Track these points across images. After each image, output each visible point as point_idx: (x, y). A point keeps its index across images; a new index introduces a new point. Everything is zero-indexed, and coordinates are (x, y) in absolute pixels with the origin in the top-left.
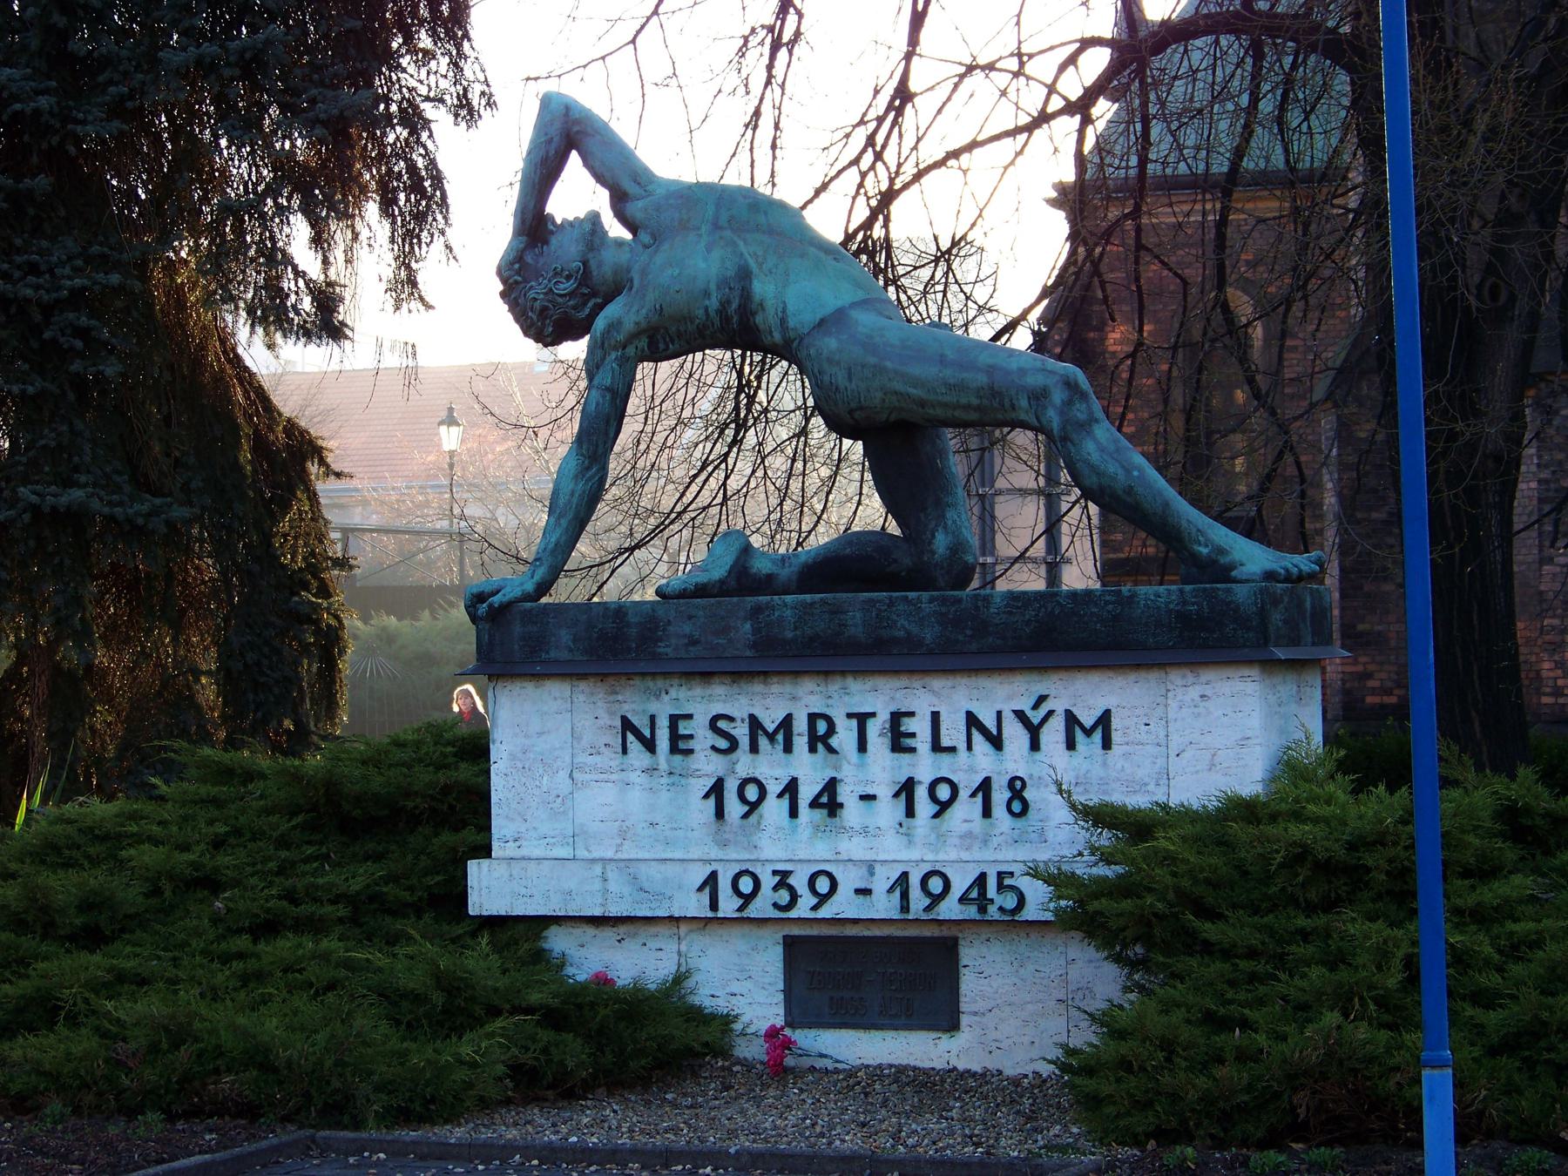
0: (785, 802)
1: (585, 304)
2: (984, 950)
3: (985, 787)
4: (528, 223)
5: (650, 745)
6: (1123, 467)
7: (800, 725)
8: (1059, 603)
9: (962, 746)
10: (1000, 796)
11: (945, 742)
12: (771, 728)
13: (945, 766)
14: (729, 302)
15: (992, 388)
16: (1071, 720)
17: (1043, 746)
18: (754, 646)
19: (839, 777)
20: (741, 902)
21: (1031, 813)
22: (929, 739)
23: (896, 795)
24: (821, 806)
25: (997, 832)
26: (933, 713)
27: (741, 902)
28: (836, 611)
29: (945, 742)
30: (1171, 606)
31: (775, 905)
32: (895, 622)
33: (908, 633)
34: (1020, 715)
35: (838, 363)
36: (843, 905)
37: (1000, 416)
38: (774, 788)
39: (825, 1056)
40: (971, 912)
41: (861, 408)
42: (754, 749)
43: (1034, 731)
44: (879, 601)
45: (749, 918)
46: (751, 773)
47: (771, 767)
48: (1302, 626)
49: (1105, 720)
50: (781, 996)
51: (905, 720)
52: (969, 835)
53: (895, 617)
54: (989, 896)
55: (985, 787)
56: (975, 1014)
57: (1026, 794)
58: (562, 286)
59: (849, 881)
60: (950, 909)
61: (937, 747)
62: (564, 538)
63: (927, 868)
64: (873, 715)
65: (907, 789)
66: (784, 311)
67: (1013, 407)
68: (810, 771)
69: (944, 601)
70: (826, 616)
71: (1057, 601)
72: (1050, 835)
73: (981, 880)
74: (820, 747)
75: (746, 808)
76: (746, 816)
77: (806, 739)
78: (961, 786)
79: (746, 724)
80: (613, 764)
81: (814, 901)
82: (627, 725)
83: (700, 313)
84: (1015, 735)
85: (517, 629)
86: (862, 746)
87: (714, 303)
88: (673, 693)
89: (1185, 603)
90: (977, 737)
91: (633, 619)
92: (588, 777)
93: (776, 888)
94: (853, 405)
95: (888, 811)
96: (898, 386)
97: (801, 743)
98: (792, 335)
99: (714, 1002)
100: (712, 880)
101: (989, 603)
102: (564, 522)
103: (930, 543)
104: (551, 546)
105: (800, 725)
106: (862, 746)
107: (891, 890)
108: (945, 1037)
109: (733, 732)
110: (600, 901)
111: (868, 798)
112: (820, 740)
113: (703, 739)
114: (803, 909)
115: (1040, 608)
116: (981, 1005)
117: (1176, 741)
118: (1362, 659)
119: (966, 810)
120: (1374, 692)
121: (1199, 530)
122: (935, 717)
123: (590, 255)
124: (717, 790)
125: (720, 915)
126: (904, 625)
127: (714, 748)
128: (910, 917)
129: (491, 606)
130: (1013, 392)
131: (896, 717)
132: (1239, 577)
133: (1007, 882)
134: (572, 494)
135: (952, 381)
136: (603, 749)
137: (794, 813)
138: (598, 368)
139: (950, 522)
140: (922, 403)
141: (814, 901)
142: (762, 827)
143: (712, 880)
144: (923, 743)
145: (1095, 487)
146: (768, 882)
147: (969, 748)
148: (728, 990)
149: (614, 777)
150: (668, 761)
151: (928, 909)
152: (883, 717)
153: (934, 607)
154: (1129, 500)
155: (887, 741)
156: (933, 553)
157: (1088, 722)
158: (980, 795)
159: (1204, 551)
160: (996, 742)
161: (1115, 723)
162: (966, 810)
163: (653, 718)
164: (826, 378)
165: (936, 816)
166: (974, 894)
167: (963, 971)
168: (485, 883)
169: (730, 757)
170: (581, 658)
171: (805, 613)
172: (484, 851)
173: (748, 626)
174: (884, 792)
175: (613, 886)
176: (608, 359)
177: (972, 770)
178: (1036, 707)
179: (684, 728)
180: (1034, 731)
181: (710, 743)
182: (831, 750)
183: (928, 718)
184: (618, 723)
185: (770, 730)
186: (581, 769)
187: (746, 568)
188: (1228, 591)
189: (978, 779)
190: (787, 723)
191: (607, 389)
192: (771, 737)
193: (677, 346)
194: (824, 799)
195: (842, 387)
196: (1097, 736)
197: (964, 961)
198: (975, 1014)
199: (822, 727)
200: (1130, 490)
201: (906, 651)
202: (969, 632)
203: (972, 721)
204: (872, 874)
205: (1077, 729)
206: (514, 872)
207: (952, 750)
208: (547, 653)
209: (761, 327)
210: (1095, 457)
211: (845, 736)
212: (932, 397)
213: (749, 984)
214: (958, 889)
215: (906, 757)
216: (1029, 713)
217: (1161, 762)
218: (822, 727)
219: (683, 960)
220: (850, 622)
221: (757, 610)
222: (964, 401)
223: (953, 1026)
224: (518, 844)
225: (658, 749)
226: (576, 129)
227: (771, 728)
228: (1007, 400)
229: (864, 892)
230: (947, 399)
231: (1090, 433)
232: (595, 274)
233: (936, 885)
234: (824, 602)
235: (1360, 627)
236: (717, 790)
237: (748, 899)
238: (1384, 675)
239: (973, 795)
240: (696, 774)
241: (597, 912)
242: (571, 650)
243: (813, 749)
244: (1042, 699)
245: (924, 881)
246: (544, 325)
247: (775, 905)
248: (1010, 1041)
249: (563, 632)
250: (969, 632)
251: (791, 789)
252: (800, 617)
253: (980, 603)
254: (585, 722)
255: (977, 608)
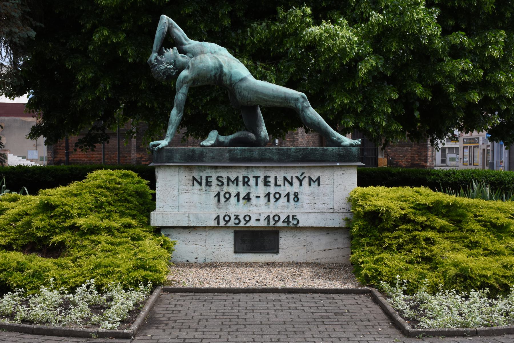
0: (236, 198)
2: (286, 234)
3: (288, 195)
7: (241, 179)
9: (282, 185)
10: (292, 197)
11: (278, 184)
12: (233, 180)
13: (278, 189)
14: (217, 73)
16: (310, 179)
17: (303, 185)
19: (250, 192)
20: (225, 223)
21: (299, 201)
22: (274, 183)
23: (265, 196)
25: (291, 205)
27: (225, 223)
28: (251, 151)
29: (278, 184)
31: (235, 223)
34: (297, 177)
35: (246, 90)
36: (253, 223)
38: (233, 195)
40: (285, 225)
42: (228, 185)
43: (301, 182)
45: (229, 227)
46: (227, 191)
47: (233, 189)
48: (160, 146)
49: (318, 179)
50: (233, 245)
52: (284, 206)
54: (290, 221)
55: (288, 195)
56: (283, 249)
57: (299, 196)
59: (254, 217)
60: (280, 224)
61: (276, 185)
63: (274, 214)
64: (260, 177)
65: (268, 195)
67: (290, 103)
68: (243, 191)
72: (304, 206)
73: (288, 217)
74: (246, 185)
75: (226, 200)
76: (225, 201)
77: (242, 182)
78: (282, 194)
80: (190, 188)
81: (245, 222)
82: (194, 179)
83: (209, 75)
84: (296, 182)
86: (257, 184)
87: (213, 73)
88: (207, 171)
89: (340, 151)
90: (286, 183)
92: (183, 191)
93: (235, 219)
94: (248, 100)
95: (263, 200)
96: (261, 96)
97: (241, 183)
98: (232, 82)
100: (218, 217)
102: (174, 127)
104: (171, 133)
105: (241, 179)
106: (257, 184)
107: (265, 220)
108: (275, 255)
109: (223, 181)
110: (187, 222)
111: (258, 197)
112: (246, 183)
113: (214, 182)
114: (242, 224)
116: (284, 247)
117: (336, 184)
118: (141, 154)
119: (283, 200)
120: (144, 161)
122: (276, 178)
124: (218, 195)
125: (220, 226)
126: (268, 155)
128: (270, 226)
129: (159, 148)
131: (266, 178)
133: (295, 217)
134: (176, 120)
136: (187, 184)
137: (238, 200)
138: (181, 88)
141: (245, 222)
143: (218, 217)
144: (272, 183)
146: (233, 218)
147: (284, 185)
148: (219, 244)
149: (190, 191)
151: (274, 224)
152: (262, 177)
153: (277, 151)
157: (314, 179)
159: (335, 138)
160: (291, 184)
161: (321, 179)
162: (283, 200)
163: (201, 177)
164: (242, 94)
166: (286, 220)
167: (280, 239)
168: (155, 218)
169: (221, 187)
173: (228, 155)
174: (262, 196)
175: (191, 219)
176: (184, 86)
177: (285, 190)
178: (301, 175)
179: (209, 179)
180: (301, 182)
181: (216, 183)
182: (249, 185)
183: (274, 178)
184: (192, 178)
186: (181, 190)
189: (286, 193)
190: (237, 179)
191: (184, 94)
192: (233, 182)
195: (246, 96)
196: (316, 183)
197: (280, 236)
198: (283, 249)
199: (246, 180)
203: (285, 179)
206: (164, 216)
207: (280, 185)
211: (252, 182)
213: (224, 243)
215: (268, 187)
216: (299, 177)
217: (332, 189)
218: (246, 180)
221: (230, 151)
222: (278, 100)
227: (233, 180)
229: (258, 220)
230: (274, 100)
231: (308, 109)
233: (277, 218)
234: (248, 149)
235: (141, 147)
236: (218, 195)
237: (227, 222)
238: (145, 158)
239: (285, 196)
240: (213, 191)
241: (187, 225)
242: (180, 160)
243: (244, 185)
244: (303, 174)
246: (164, 76)
247: (235, 223)
248: (292, 255)
249: (178, 155)
251: (238, 195)
254: (188, 177)
255: (288, 151)
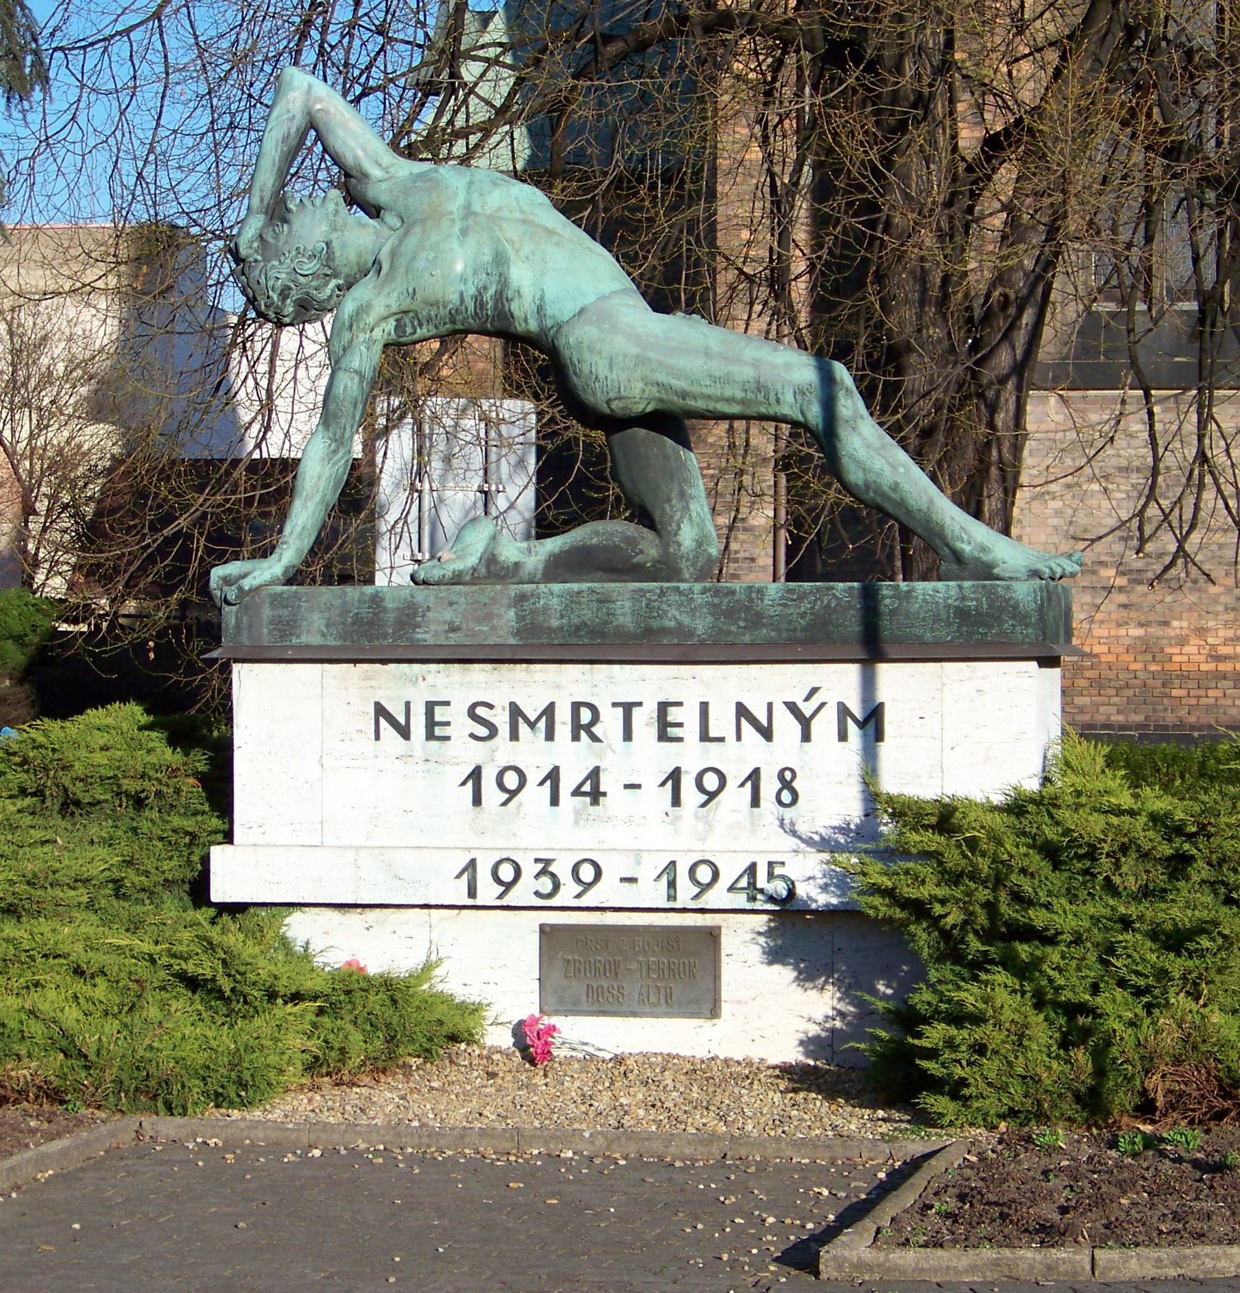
1: (326, 285)
3: (755, 776)
4: (266, 202)
5: (405, 732)
6: (890, 464)
7: (563, 716)
8: (835, 596)
9: (731, 735)
10: (769, 786)
11: (713, 733)
13: (713, 755)
14: (485, 288)
15: (758, 382)
18: (517, 634)
24: (585, 794)
26: (702, 703)
28: (604, 600)
29: (712, 734)
30: (950, 601)
31: (537, 893)
32: (665, 612)
33: (680, 624)
34: (792, 707)
37: (763, 410)
38: (534, 777)
39: (586, 1044)
41: (620, 398)
42: (514, 736)
43: (805, 723)
44: (649, 591)
51: (671, 710)
53: (665, 607)
55: (755, 776)
57: (794, 784)
58: (306, 267)
60: (718, 897)
61: (705, 737)
62: (310, 521)
66: (542, 299)
69: (717, 592)
70: (595, 605)
71: (834, 595)
73: (752, 870)
74: (583, 734)
77: (569, 727)
79: (507, 712)
82: (381, 711)
83: (455, 298)
84: (786, 726)
85: (267, 612)
86: (628, 735)
89: (963, 599)
91: (390, 605)
94: (612, 395)
96: (662, 378)
99: (466, 991)
101: (763, 595)
103: (676, 534)
105: (563, 716)
106: (628, 735)
109: (492, 720)
113: (461, 726)
115: (815, 601)
119: (736, 797)
121: (962, 528)
122: (704, 707)
123: (334, 236)
126: (674, 616)
127: (473, 736)
130: (779, 387)
132: (1002, 575)
133: (778, 871)
134: (319, 478)
135: (717, 374)
137: (555, 801)
139: (694, 515)
140: (684, 395)
142: (522, 815)
145: (860, 483)
146: (530, 869)
147: (739, 738)
150: (424, 748)
153: (707, 598)
154: (893, 496)
155: (654, 731)
156: (679, 545)
158: (548, 783)
160: (767, 733)
165: (704, 805)
166: (744, 883)
170: (334, 643)
171: (572, 602)
172: (228, 838)
173: (512, 613)
178: (807, 699)
180: (805, 723)
182: (595, 738)
185: (532, 719)
187: (494, 555)
188: (1008, 588)
192: (532, 725)
193: (425, 330)
194: (587, 788)
195: (601, 376)
199: (586, 716)
200: (895, 487)
201: (676, 641)
202: (742, 624)
203: (742, 711)
204: (638, 863)
205: (849, 720)
208: (298, 637)
209: (516, 313)
210: (862, 454)
211: (611, 723)
212: (696, 389)
214: (726, 880)
219: (434, 948)
220: (619, 612)
221: (522, 597)
222: (728, 393)
223: (714, 1012)
224: (262, 830)
225: (412, 736)
226: (318, 106)
228: (772, 394)
232: (337, 254)
242: (324, 635)
243: (576, 737)
245: (692, 870)
247: (537, 893)
250: (742, 624)
251: (553, 776)
252: (566, 606)
253: (754, 595)
255: (751, 600)
